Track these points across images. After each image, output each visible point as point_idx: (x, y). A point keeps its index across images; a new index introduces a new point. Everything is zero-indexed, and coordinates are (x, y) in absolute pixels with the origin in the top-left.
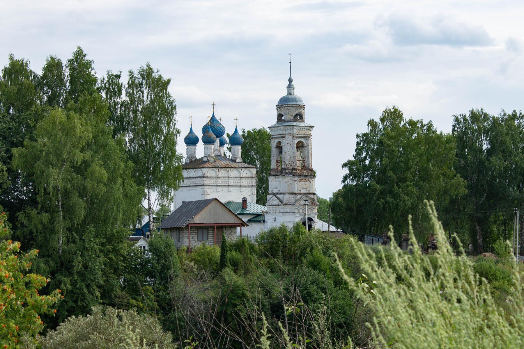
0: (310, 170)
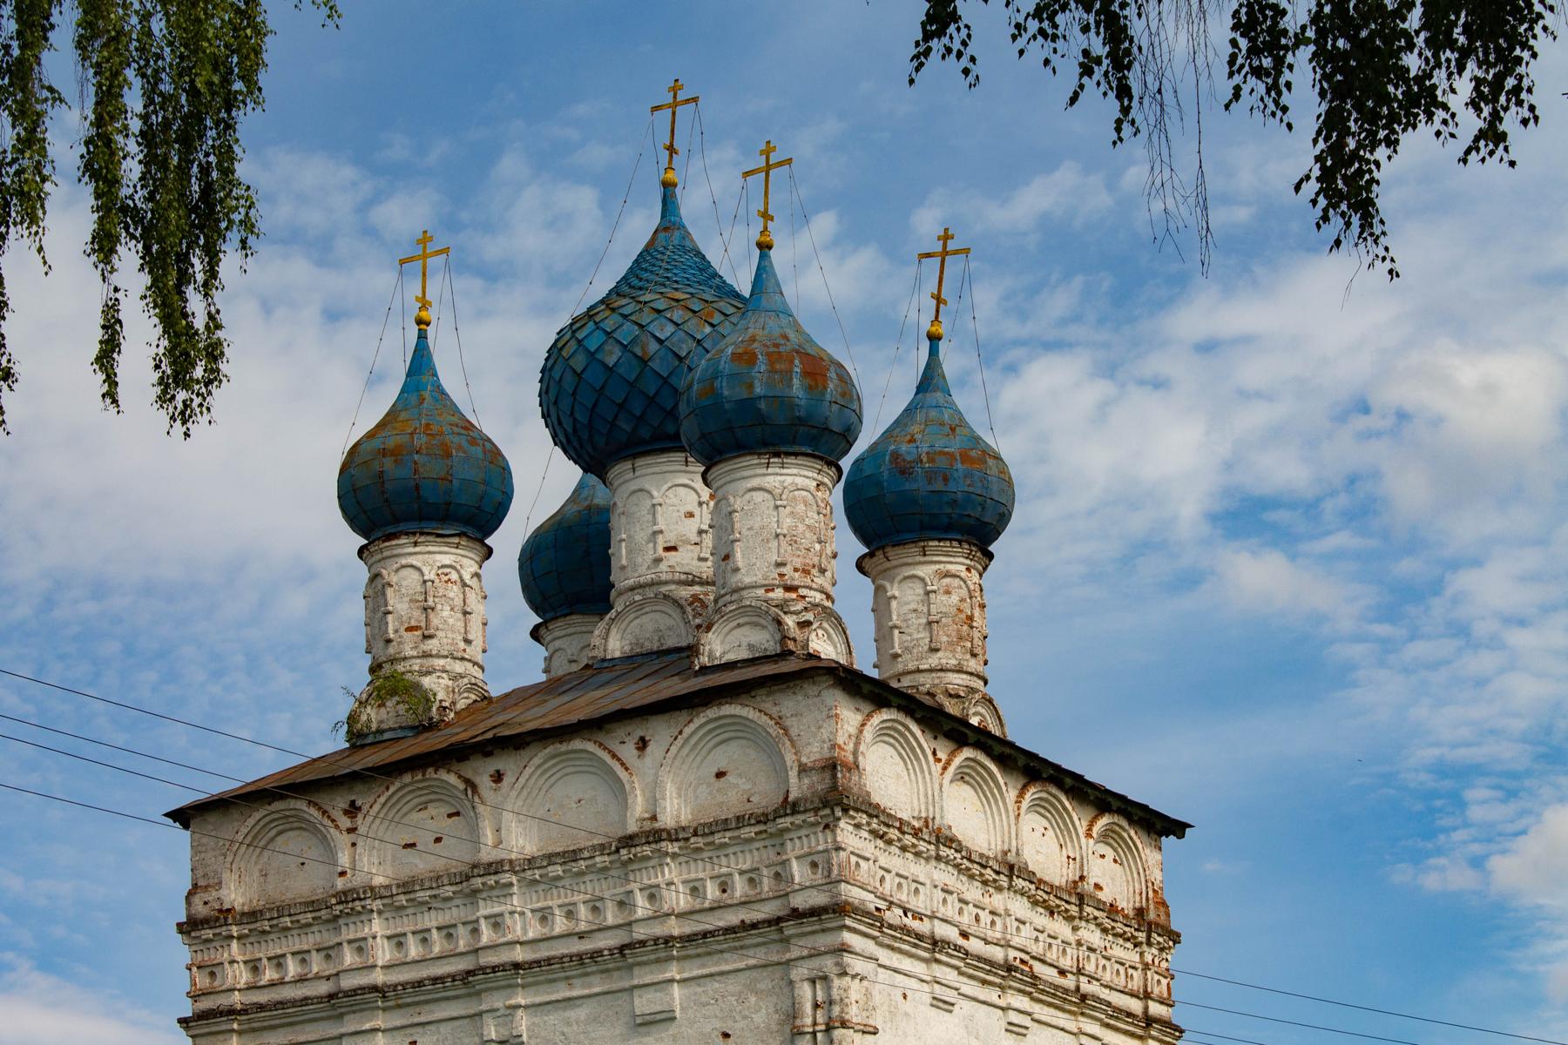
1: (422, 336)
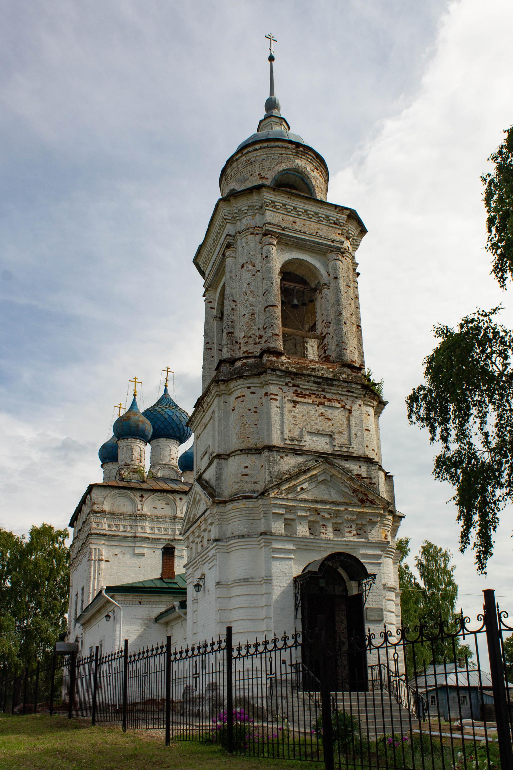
0: (351, 366)
1: (135, 398)
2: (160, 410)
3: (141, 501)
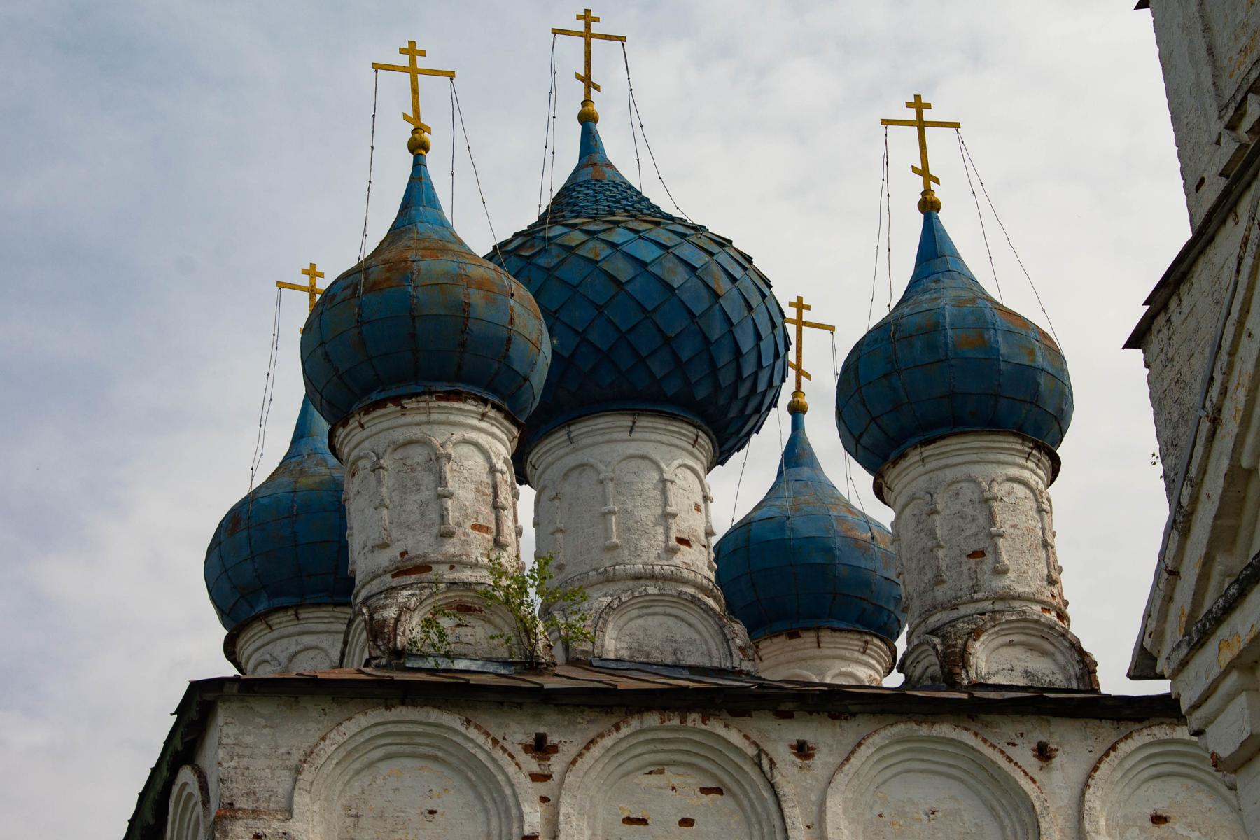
1: (418, 164)
2: (577, 237)
3: (535, 777)
